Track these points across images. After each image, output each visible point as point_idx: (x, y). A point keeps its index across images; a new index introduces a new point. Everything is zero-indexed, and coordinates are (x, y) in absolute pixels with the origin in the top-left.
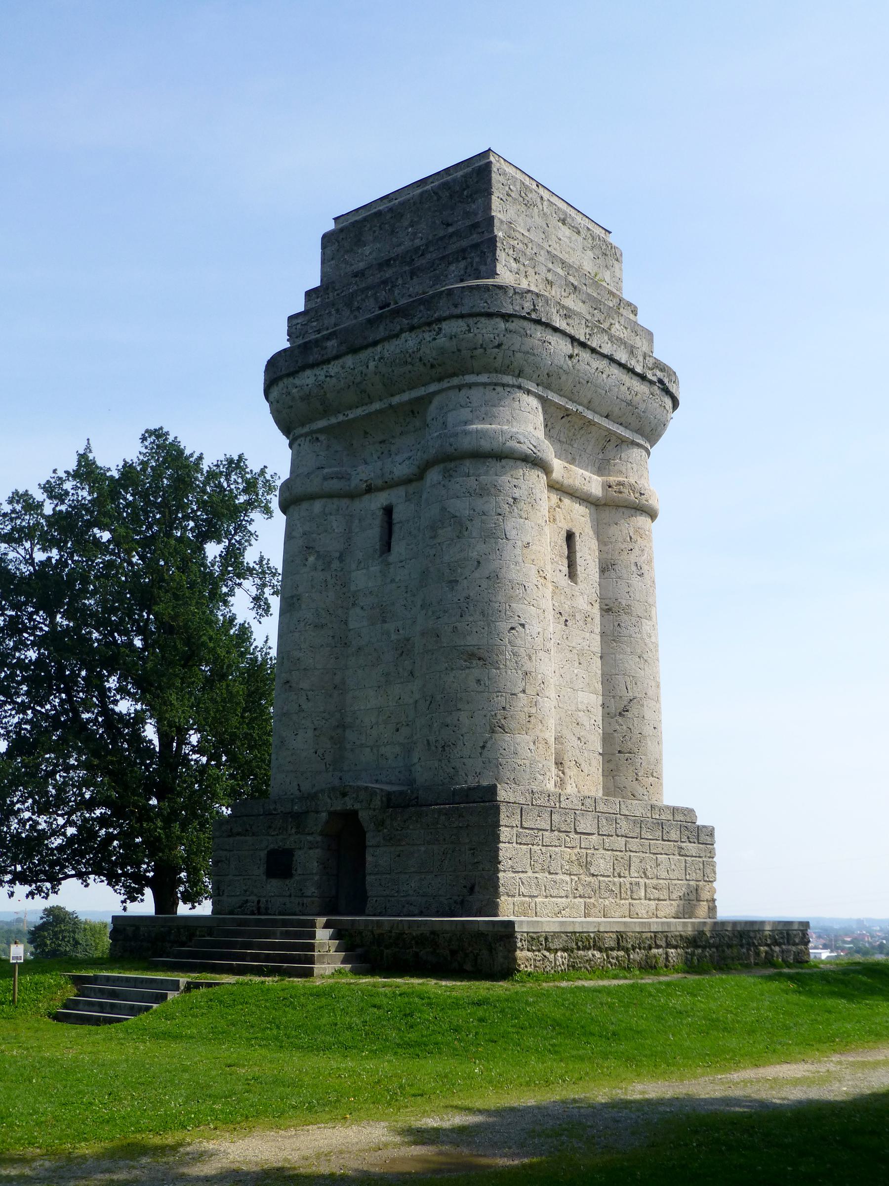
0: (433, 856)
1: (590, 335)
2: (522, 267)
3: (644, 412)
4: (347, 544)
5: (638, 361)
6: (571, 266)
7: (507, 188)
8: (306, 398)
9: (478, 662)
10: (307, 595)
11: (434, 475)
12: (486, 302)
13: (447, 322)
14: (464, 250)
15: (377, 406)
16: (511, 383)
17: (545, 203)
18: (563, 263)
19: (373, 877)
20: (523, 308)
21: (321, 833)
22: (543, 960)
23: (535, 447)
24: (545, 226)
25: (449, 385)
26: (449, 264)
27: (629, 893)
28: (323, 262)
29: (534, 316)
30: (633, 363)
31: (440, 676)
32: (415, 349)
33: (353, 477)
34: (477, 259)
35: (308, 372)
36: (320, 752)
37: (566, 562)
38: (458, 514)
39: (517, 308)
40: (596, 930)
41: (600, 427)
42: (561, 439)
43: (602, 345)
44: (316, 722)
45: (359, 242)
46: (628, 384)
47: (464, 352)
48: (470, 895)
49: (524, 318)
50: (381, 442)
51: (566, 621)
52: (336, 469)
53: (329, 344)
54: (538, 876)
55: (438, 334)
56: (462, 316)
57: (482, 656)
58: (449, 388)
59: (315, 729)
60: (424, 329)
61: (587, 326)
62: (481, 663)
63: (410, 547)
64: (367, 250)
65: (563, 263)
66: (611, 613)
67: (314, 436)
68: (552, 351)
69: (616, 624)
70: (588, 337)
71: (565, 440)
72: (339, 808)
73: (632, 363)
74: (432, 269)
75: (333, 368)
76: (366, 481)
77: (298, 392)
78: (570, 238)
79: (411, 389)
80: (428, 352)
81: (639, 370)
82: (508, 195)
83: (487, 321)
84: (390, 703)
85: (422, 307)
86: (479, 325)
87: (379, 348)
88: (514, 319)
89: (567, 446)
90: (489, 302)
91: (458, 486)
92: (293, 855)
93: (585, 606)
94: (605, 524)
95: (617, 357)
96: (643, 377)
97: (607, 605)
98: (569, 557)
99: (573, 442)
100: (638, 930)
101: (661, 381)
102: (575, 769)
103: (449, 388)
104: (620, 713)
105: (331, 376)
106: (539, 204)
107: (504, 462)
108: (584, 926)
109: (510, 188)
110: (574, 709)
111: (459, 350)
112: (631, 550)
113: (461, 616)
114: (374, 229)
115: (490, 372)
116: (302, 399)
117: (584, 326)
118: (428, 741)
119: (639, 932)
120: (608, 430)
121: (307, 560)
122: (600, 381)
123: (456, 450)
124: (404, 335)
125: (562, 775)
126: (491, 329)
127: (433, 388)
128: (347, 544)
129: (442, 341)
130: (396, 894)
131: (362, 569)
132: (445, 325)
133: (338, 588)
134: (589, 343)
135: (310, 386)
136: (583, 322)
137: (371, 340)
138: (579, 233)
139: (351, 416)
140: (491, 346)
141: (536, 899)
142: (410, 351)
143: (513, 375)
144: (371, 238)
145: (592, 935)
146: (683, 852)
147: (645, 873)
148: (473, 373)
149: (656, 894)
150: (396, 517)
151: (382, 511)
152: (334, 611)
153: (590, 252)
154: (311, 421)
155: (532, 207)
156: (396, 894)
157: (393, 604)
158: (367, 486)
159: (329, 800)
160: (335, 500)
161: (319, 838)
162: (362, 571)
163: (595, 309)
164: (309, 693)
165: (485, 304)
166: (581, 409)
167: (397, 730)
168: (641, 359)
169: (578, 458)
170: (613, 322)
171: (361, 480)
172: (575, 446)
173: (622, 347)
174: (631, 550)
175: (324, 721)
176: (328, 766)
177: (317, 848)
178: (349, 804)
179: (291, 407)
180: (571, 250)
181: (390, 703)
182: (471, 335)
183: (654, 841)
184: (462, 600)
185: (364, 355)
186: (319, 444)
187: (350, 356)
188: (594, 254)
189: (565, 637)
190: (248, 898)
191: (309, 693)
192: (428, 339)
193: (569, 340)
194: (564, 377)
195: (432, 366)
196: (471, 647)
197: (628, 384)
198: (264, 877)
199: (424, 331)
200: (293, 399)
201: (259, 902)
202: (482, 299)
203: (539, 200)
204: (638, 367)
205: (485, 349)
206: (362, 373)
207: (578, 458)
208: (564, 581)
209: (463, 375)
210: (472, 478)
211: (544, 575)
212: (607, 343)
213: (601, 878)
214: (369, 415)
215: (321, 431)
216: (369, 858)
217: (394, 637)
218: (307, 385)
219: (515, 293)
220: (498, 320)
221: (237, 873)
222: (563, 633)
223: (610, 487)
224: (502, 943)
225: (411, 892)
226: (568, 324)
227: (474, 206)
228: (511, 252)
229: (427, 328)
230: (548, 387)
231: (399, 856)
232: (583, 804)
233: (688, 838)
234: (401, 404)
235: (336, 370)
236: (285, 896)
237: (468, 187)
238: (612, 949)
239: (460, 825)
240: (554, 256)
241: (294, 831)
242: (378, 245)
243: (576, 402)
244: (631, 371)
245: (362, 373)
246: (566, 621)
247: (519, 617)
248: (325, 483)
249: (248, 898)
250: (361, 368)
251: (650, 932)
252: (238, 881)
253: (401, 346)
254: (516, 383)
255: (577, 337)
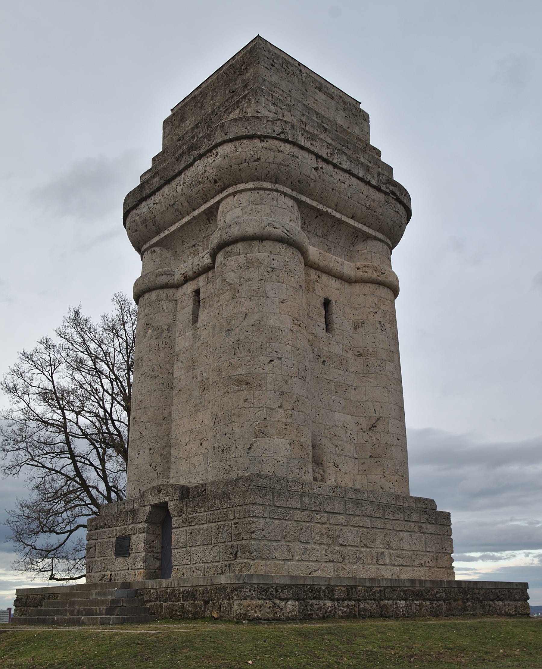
0: (212, 532)
1: (331, 154)
2: (279, 110)
3: (381, 215)
4: (173, 319)
5: (373, 177)
6: (324, 117)
7: (271, 61)
8: (144, 222)
9: (246, 386)
10: (146, 356)
11: (219, 258)
12: (246, 128)
13: (221, 147)
14: (238, 102)
15: (186, 219)
16: (270, 187)
17: (304, 75)
18: (317, 115)
19: (176, 551)
20: (274, 131)
21: (147, 522)
22: (274, 607)
23: (288, 231)
24: (304, 91)
25: (227, 193)
26: (230, 113)
27: (375, 560)
28: (164, 139)
29: (282, 136)
30: (369, 177)
31: (221, 399)
32: (203, 171)
33: (176, 273)
34: (245, 105)
35: (144, 203)
36: (153, 466)
37: (323, 320)
38: (232, 282)
39: (269, 131)
40: (326, 583)
41: (348, 225)
42: (318, 234)
43: (342, 162)
44: (151, 444)
45: (183, 119)
46: (366, 193)
47: (234, 167)
48: (235, 559)
49: (275, 138)
50: (193, 246)
51: (324, 361)
52: (165, 269)
53: (154, 180)
54: (290, 544)
55: (216, 156)
56: (231, 141)
57: (249, 382)
58: (227, 196)
59: (150, 449)
60: (208, 155)
61: (329, 148)
62: (248, 386)
63: (209, 314)
64: (188, 123)
65: (317, 115)
66: (361, 357)
67: (152, 249)
68: (300, 163)
69: (365, 365)
70: (329, 155)
71: (321, 235)
72: (157, 502)
73: (369, 177)
74: (219, 120)
75: (157, 197)
76: (184, 274)
77: (139, 219)
78: (325, 101)
79: (205, 203)
80: (211, 171)
81: (374, 182)
82: (272, 65)
83: (248, 142)
84: (197, 426)
85: (206, 140)
86: (243, 146)
87: (183, 175)
88: (268, 140)
89: (323, 239)
90: (249, 128)
91: (232, 263)
92: (130, 539)
93: (341, 352)
94: (356, 295)
95: (353, 171)
96: (379, 189)
97: (359, 352)
98: (325, 317)
99: (328, 237)
100: (368, 584)
101: (393, 193)
102: (334, 469)
103: (227, 196)
104: (370, 428)
105: (157, 203)
106: (298, 75)
107: (265, 242)
108: (315, 580)
109: (273, 61)
110: (332, 425)
111: (231, 166)
112: (376, 313)
113: (235, 354)
114: (191, 108)
115: (254, 181)
116: (142, 223)
117: (325, 147)
118: (214, 447)
119: (369, 587)
120: (354, 228)
121: (147, 333)
122: (342, 189)
123: (230, 237)
124: (196, 163)
125: (322, 473)
126: (251, 148)
127: (217, 199)
128: (173, 319)
129: (219, 160)
130: (189, 563)
131: (182, 335)
132: (220, 149)
133: (167, 350)
134: (330, 159)
135: (145, 213)
136: (325, 144)
137: (176, 171)
138: (332, 98)
139: (172, 230)
140: (252, 160)
141: (289, 563)
142: (201, 173)
143: (271, 182)
144: (190, 114)
145: (323, 588)
146: (423, 530)
147: (388, 545)
148: (242, 182)
149: (399, 561)
150: (201, 296)
151: (194, 293)
152: (164, 366)
153: (342, 112)
154: (150, 239)
155: (293, 76)
156: (189, 563)
157: (199, 356)
158: (184, 278)
159: (151, 497)
160: (165, 290)
161: (145, 525)
162: (182, 336)
163: (343, 146)
164: (147, 424)
165: (246, 130)
166: (330, 210)
167: (201, 444)
168: (376, 176)
169: (333, 248)
170: (359, 156)
171: (181, 274)
172: (330, 239)
173: (359, 166)
174: (376, 313)
175: (156, 443)
176: (159, 475)
177: (144, 532)
178: (162, 498)
179: (137, 231)
180: (326, 109)
181: (197, 426)
182: (237, 153)
183: (397, 522)
184: (235, 343)
185: (174, 183)
186: (155, 254)
187: (166, 186)
188: (345, 113)
189: (323, 372)
190: (105, 573)
191: (147, 424)
192: (211, 162)
193: (314, 157)
194: (312, 185)
195: (216, 182)
196: (241, 376)
197: (366, 193)
198: (114, 557)
199: (208, 157)
200: (137, 225)
201: (111, 575)
202: (243, 127)
203: (298, 72)
204: (373, 181)
205: (248, 163)
206: (174, 196)
207: (333, 248)
208: (321, 333)
209: (236, 185)
210: (242, 255)
211: (299, 324)
212: (347, 162)
213: (350, 548)
214: (182, 226)
215: (155, 245)
216: (174, 537)
217: (199, 379)
218: (144, 213)
219: (268, 121)
220: (257, 141)
221: (100, 556)
222: (321, 370)
223: (358, 269)
224: (236, 593)
225: (198, 561)
226: (311, 144)
227: (248, 75)
228: (270, 98)
229: (210, 154)
230: (301, 192)
231: (191, 533)
232: (334, 492)
233: (427, 519)
234: (199, 215)
235: (159, 198)
236: (125, 570)
237: (244, 63)
238: (343, 600)
239: (228, 506)
240: (310, 109)
241: (131, 521)
242: (194, 118)
243: (325, 205)
244: (368, 183)
245: (174, 196)
246: (324, 361)
247: (277, 352)
248: (158, 279)
249: (105, 573)
250: (173, 193)
251: (380, 587)
252: (100, 560)
253: (195, 171)
254: (274, 188)
255: (320, 154)
